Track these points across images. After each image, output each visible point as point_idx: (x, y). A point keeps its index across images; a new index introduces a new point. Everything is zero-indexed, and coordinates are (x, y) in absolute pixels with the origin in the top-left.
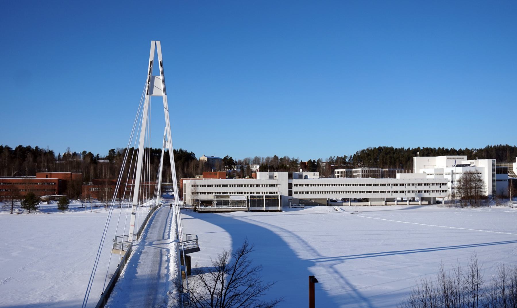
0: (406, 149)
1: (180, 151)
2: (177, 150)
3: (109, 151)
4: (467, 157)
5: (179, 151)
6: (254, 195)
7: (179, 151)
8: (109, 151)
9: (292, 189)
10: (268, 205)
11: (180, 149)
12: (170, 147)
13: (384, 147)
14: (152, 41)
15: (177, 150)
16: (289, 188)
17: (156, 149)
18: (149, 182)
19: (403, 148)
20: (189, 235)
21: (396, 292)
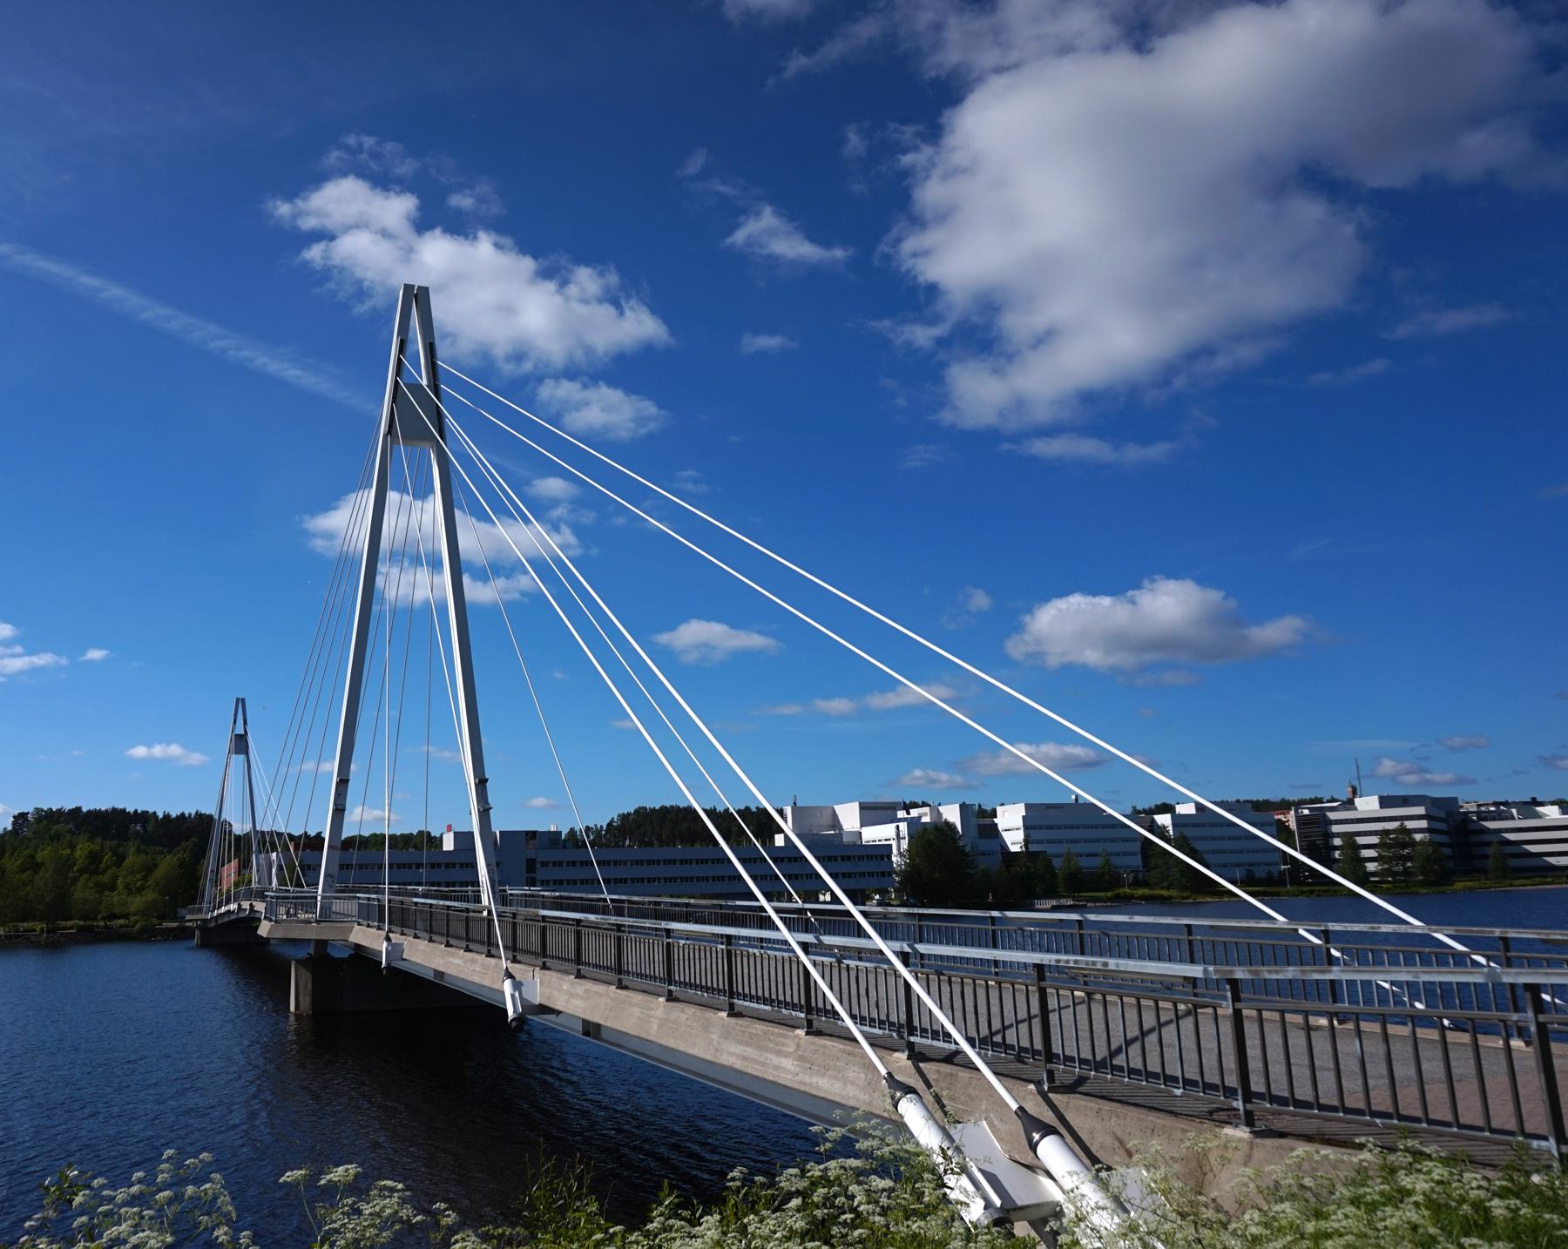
0: (720, 812)
1: (195, 817)
2: (190, 815)
3: (14, 817)
4: (782, 847)
5: (192, 816)
6: (1098, 980)
7: (192, 816)
8: (14, 817)
9: (535, 872)
10: (623, 908)
11: (197, 812)
12: (265, 830)
13: (672, 807)
14: (452, 848)
15: (190, 815)
16: (528, 871)
17: (136, 811)
18: (626, 905)
19: (715, 809)
20: (1087, 827)
21: (1337, 1137)
